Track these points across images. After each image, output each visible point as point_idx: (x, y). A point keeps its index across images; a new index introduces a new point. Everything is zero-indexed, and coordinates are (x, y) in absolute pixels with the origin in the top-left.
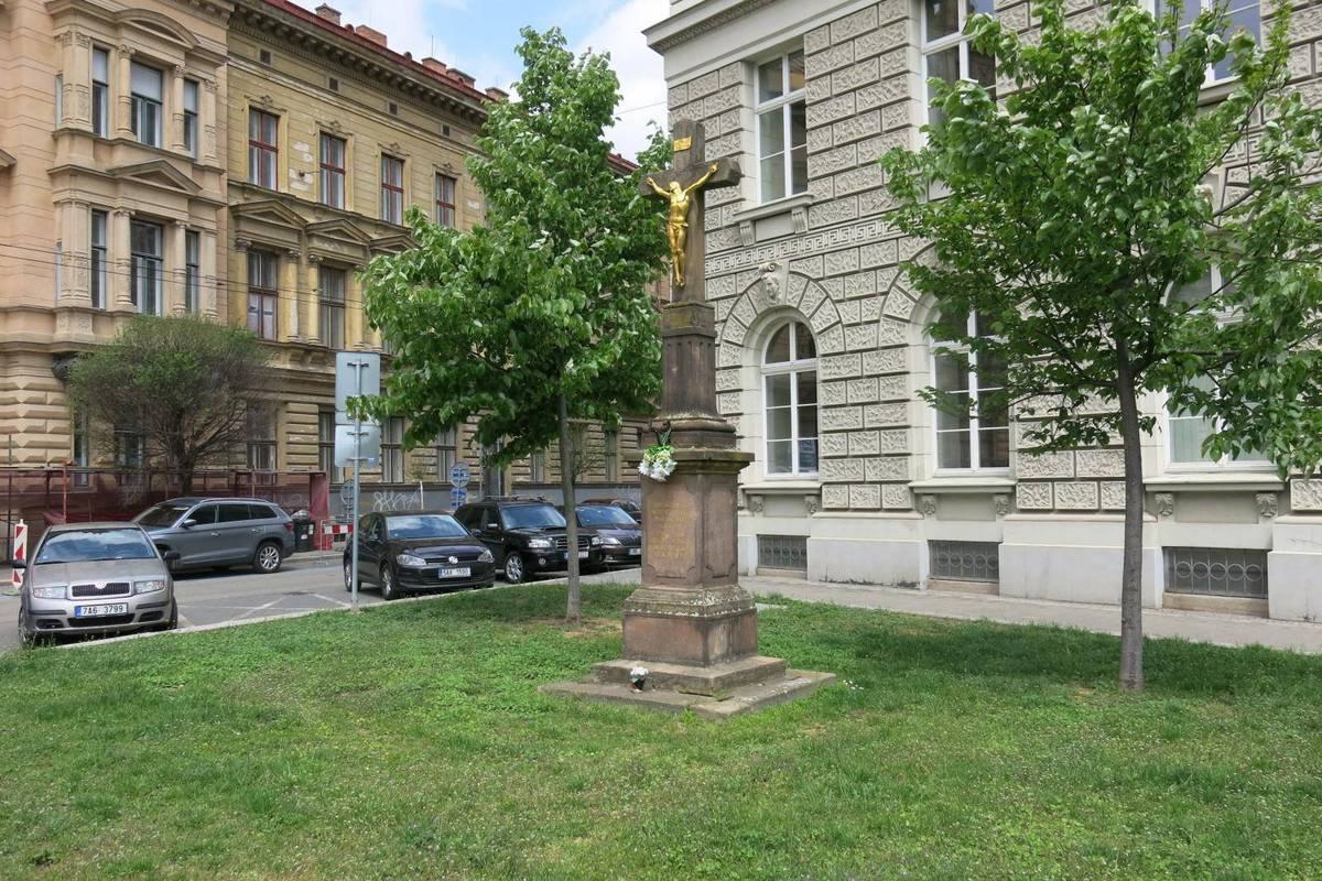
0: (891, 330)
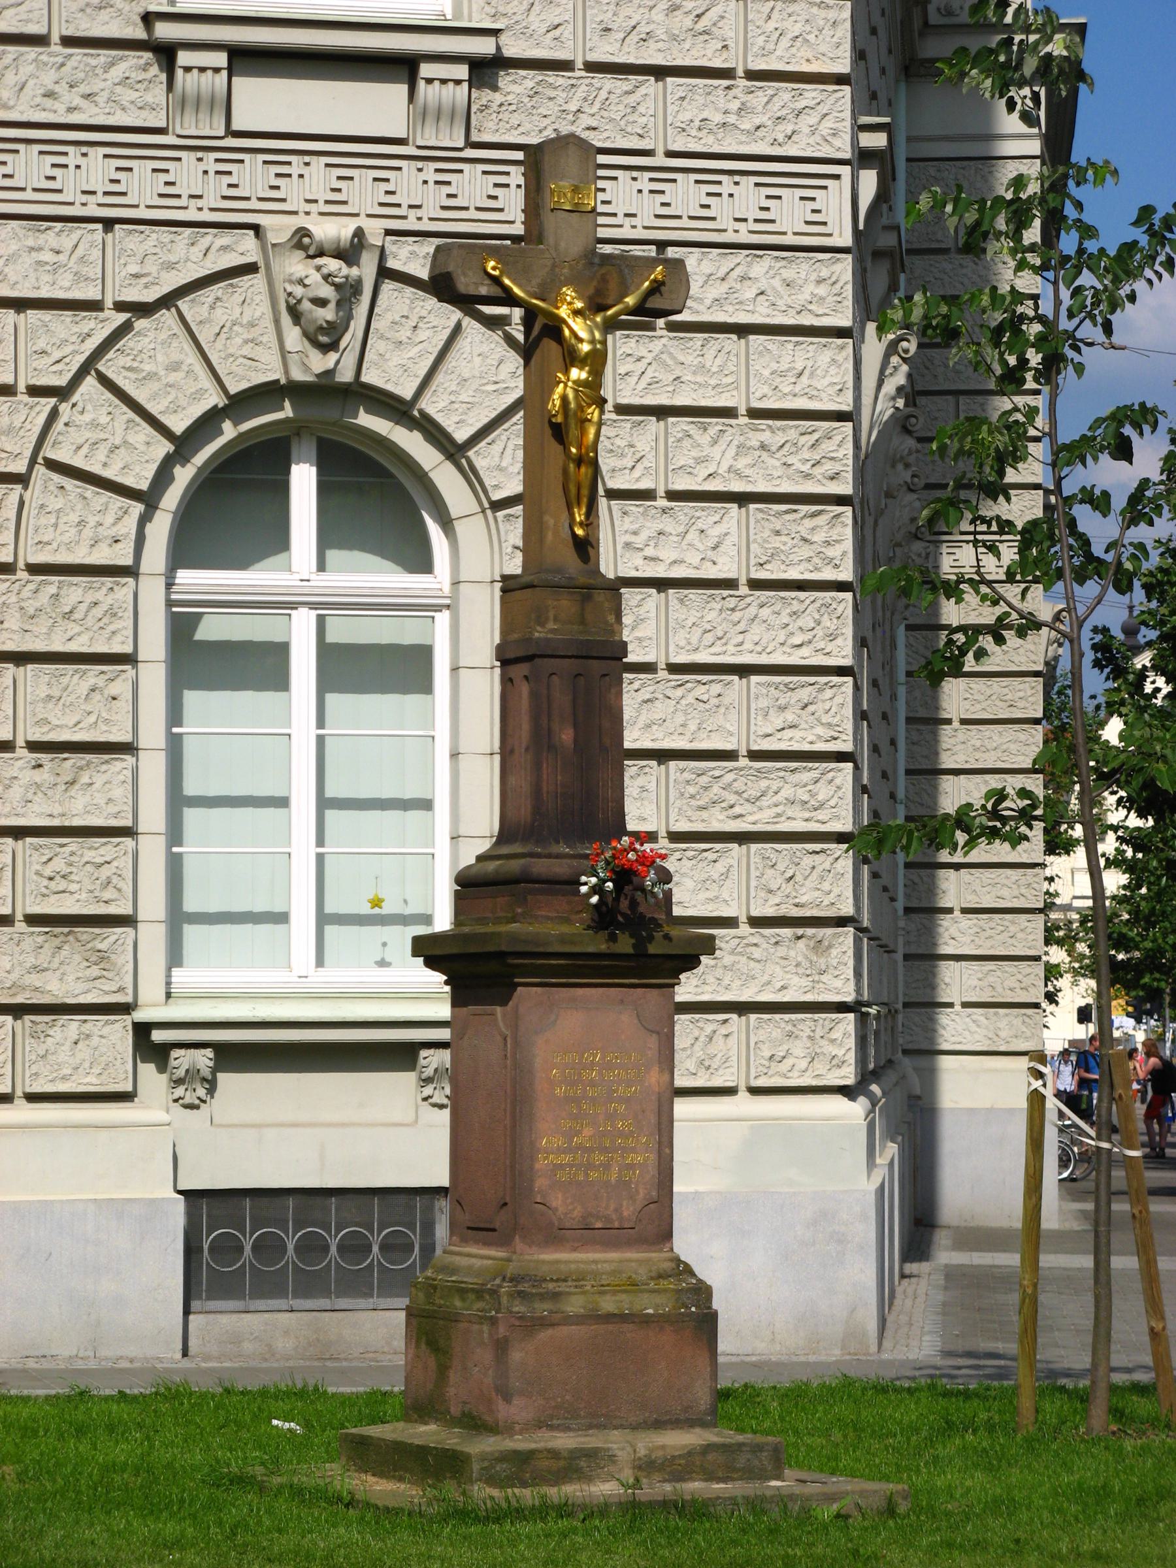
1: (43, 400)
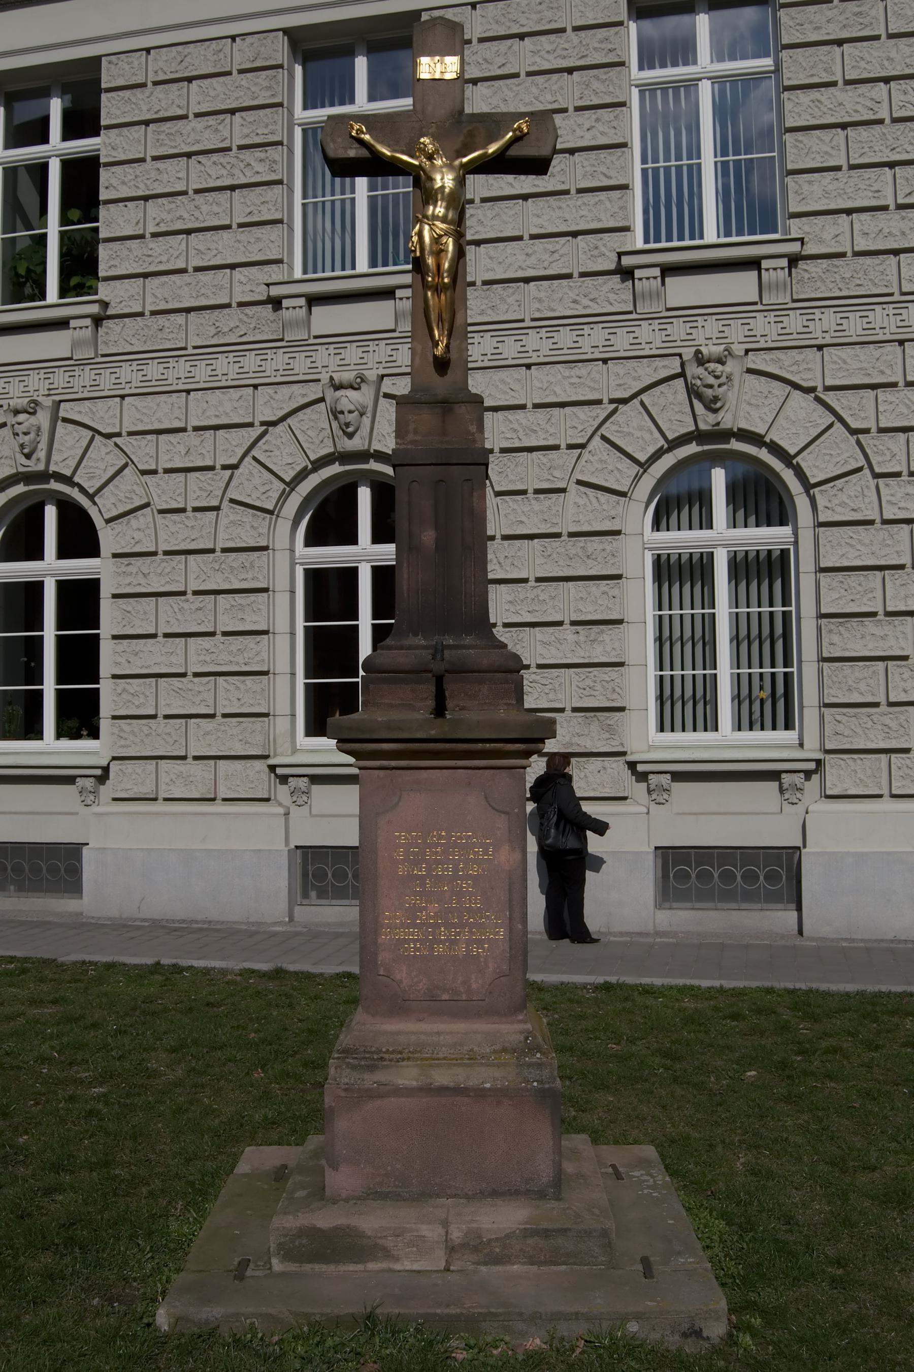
0: (241, 524)
1: (574, 451)
